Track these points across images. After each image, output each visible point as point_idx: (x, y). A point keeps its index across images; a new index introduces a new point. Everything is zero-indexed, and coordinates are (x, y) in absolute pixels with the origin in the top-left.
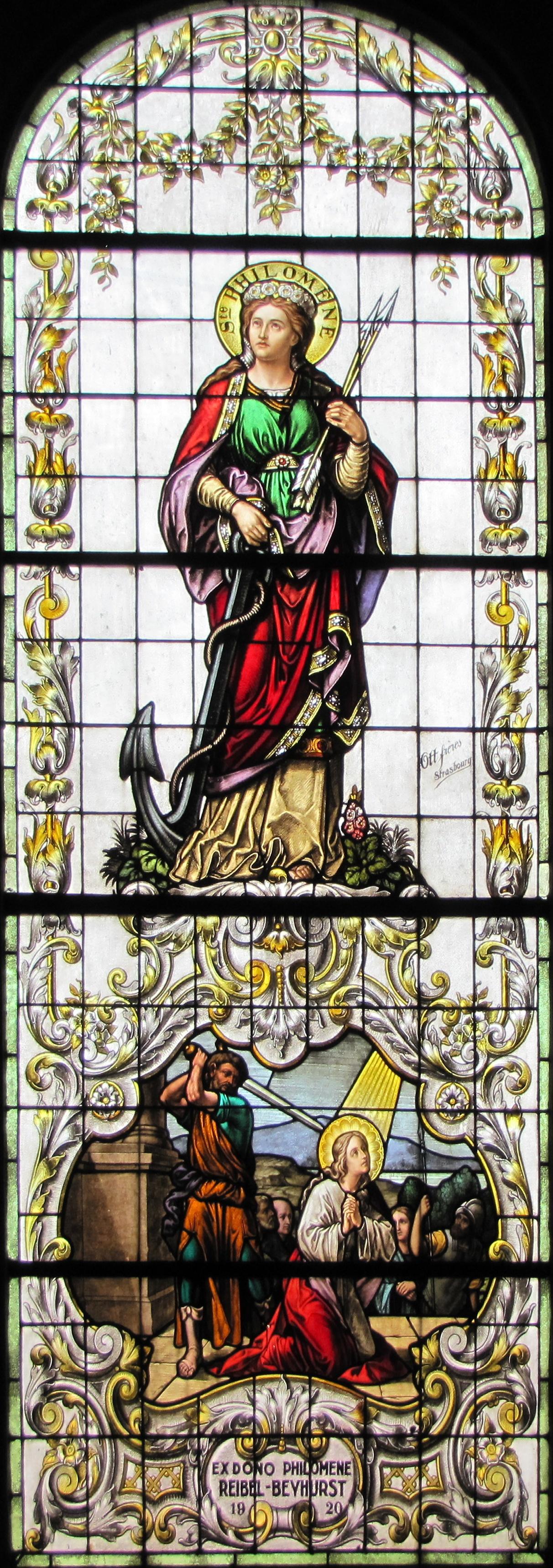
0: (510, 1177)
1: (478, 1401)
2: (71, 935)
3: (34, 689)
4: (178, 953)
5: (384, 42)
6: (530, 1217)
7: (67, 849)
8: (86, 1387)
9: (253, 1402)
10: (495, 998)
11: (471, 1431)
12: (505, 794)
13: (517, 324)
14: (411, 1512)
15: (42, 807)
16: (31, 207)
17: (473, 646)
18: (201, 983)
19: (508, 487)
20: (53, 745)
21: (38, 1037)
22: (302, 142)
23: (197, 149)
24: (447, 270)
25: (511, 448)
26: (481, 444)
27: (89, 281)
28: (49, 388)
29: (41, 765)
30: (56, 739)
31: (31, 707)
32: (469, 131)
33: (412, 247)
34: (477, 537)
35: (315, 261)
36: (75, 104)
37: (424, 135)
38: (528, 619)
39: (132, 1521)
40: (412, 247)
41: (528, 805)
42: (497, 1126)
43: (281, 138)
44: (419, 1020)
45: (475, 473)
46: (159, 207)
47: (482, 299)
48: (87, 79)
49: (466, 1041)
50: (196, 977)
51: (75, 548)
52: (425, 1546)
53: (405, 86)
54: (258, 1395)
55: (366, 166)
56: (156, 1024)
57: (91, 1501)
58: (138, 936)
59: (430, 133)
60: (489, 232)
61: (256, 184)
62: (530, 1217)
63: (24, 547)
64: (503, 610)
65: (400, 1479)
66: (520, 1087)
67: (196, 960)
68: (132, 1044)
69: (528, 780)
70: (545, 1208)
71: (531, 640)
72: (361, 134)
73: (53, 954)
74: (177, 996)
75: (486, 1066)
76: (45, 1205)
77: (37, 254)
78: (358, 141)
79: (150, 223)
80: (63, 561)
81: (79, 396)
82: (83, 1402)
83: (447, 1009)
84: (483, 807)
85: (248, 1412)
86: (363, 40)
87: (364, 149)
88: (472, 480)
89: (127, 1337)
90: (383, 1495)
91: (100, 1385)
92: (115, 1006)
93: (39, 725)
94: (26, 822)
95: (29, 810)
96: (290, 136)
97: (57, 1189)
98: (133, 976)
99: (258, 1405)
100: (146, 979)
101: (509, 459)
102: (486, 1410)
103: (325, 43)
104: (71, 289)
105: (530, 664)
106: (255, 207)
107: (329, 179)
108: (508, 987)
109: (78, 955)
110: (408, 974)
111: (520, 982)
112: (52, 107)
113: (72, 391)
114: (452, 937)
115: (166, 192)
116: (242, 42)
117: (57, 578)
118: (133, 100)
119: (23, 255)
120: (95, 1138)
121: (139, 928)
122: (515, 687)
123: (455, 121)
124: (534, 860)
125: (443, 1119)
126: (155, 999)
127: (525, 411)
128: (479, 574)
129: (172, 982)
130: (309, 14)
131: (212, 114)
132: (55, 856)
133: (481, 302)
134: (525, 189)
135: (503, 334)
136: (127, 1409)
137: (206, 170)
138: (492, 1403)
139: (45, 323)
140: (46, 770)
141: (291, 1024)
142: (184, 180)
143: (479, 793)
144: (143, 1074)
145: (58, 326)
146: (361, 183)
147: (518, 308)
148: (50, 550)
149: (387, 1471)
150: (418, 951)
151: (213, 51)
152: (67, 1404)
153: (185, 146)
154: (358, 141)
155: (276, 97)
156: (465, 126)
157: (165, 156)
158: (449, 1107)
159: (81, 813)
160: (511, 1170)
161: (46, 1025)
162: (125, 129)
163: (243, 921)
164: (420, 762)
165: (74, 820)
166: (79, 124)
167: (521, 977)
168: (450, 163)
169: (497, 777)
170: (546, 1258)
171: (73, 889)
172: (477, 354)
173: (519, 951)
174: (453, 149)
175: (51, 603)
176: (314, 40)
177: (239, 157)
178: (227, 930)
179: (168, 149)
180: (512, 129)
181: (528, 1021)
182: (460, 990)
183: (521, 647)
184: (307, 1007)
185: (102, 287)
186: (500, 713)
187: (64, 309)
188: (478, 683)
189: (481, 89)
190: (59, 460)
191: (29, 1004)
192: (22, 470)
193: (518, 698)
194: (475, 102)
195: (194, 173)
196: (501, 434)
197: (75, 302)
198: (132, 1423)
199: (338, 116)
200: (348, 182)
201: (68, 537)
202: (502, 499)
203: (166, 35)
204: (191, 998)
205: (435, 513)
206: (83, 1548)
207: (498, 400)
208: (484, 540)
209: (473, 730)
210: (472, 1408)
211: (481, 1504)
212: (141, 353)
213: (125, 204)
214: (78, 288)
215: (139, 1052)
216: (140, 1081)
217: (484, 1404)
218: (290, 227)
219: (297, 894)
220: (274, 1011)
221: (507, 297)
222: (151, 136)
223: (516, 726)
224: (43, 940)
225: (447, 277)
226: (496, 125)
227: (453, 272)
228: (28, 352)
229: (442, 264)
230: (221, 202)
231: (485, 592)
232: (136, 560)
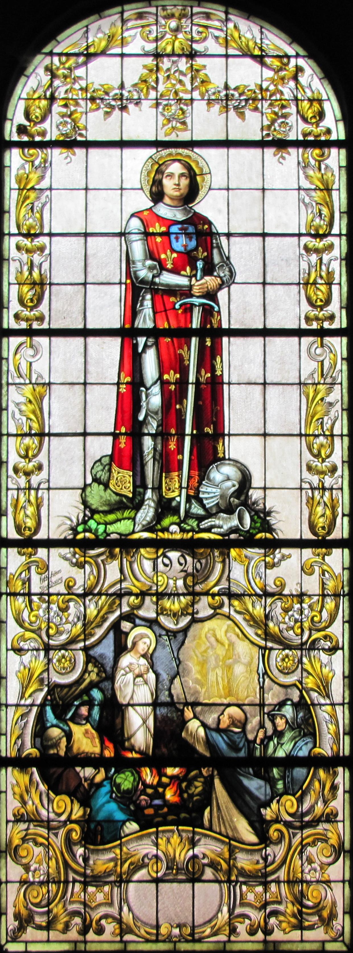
7: (38, 507)
8: (48, 834)
9: (157, 845)
16: (17, 317)
18: (124, 585)
19: (323, 288)
21: (20, 622)
22: (192, 89)
34: (303, 317)
36: (49, 69)
39: (78, 920)
41: (336, 475)
48: (57, 50)
50: (121, 581)
52: (269, 938)
53: (257, 52)
54: (160, 840)
57: (51, 907)
61: (163, 115)
63: (14, 325)
65: (253, 894)
67: (122, 571)
68: (80, 625)
72: (229, 83)
73: (29, 569)
75: (310, 636)
78: (227, 87)
81: (51, 235)
82: (46, 843)
90: (242, 905)
91: (57, 833)
98: (80, 582)
99: (160, 847)
100: (89, 582)
101: (324, 268)
102: (309, 848)
106: (162, 129)
107: (208, 111)
112: (34, 70)
115: (105, 120)
122: (328, 399)
129: (105, 586)
130: (196, 10)
131: (134, 70)
132: (30, 510)
134: (332, 109)
136: (75, 848)
137: (131, 107)
138: (313, 844)
140: (26, 456)
143: (304, 468)
144: (87, 643)
146: (229, 113)
152: (36, 843)
153: (117, 91)
154: (227, 87)
155: (175, 59)
156: (295, 78)
162: (80, 82)
166: (51, 79)
167: (332, 582)
169: (315, 456)
170: (347, 752)
172: (304, 202)
174: (286, 91)
182: (291, 588)
188: (303, 397)
192: (13, 280)
194: (301, 62)
195: (123, 108)
198: (78, 857)
199: (214, 70)
200: (221, 113)
201: (41, 319)
206: (45, 938)
208: (308, 319)
211: (304, 910)
212: (88, 209)
217: (308, 844)
218: (185, 136)
222: (96, 86)
230: (142, 122)
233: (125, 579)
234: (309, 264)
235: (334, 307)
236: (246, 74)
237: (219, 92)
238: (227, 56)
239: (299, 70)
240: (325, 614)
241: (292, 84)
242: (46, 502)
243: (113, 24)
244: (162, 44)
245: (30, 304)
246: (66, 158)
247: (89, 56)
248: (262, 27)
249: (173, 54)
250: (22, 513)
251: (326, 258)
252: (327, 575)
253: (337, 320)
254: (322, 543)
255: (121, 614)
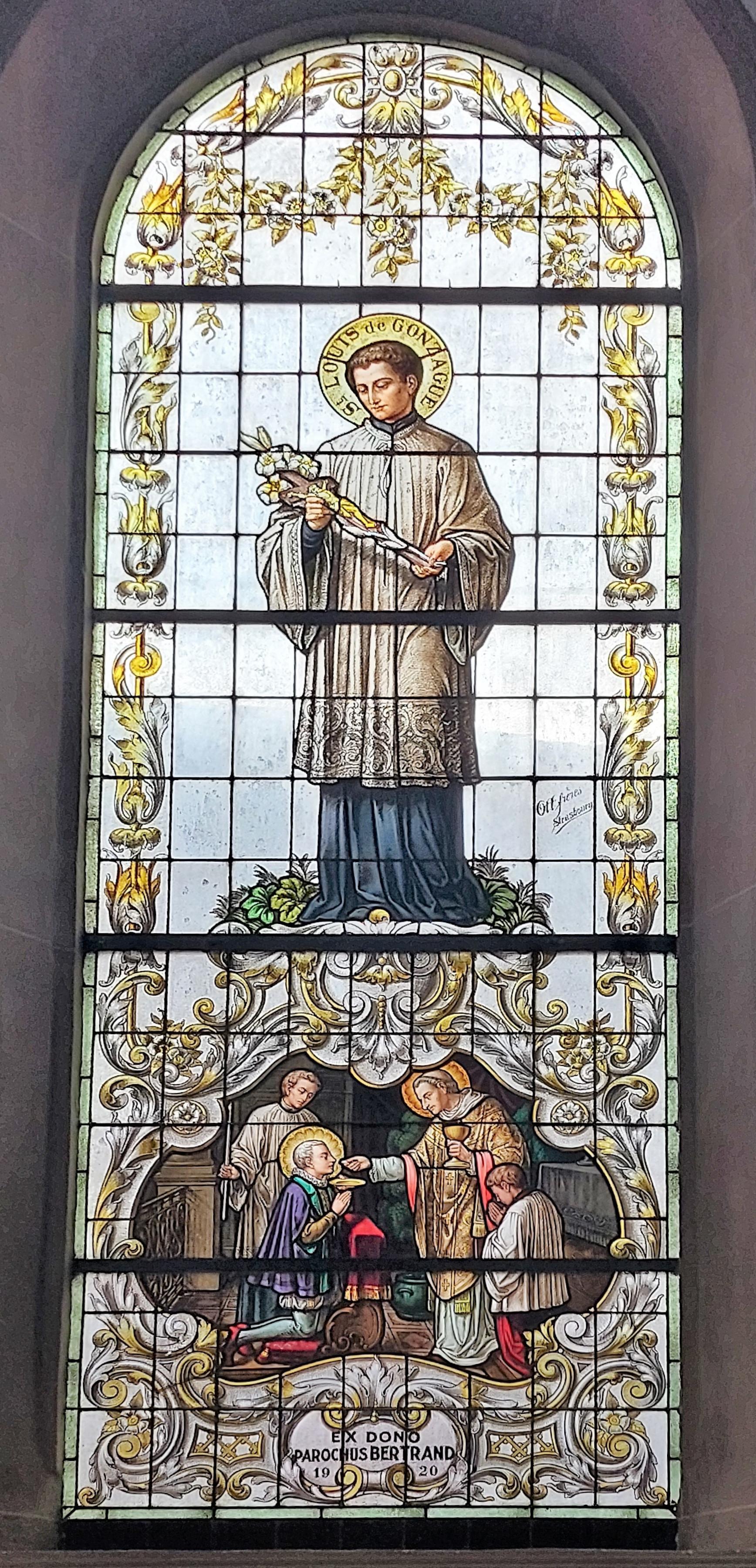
0: (633, 1183)
1: (598, 1379)
2: (154, 970)
3: (120, 743)
4: (272, 985)
5: (513, 83)
6: (658, 1218)
10: (618, 1023)
11: (592, 1404)
12: (627, 838)
13: (649, 377)
14: (524, 1474)
15: (127, 854)
17: (596, 698)
20: (140, 794)
23: (310, 200)
24: (575, 321)
25: (641, 502)
26: (609, 500)
27: (192, 335)
28: (145, 444)
29: (127, 815)
30: (143, 790)
31: (118, 760)
32: (600, 177)
33: (537, 297)
35: (434, 314)
37: (552, 180)
38: (656, 669)
40: (537, 297)
42: (621, 1139)
43: (398, 187)
44: (534, 1043)
45: (601, 529)
46: (268, 260)
47: (610, 349)
49: (584, 1062)
51: (168, 605)
53: (532, 129)
55: (489, 214)
56: (245, 1049)
58: (227, 970)
59: (558, 178)
60: (621, 282)
62: (658, 1218)
63: (114, 603)
64: (629, 661)
66: (647, 1104)
69: (655, 824)
70: (675, 1207)
71: (658, 691)
72: (484, 181)
73: (134, 986)
74: (266, 1026)
76: (117, 1209)
77: (136, 306)
78: (481, 188)
79: (255, 275)
80: (156, 618)
83: (565, 1034)
84: (604, 850)
85: (337, 1387)
86: (488, 76)
87: (487, 196)
88: (597, 536)
89: (203, 1322)
92: (202, 1032)
93: (126, 778)
94: (109, 870)
95: (112, 857)
96: (408, 183)
97: (129, 1199)
103: (447, 82)
104: (172, 342)
105: (657, 716)
108: (632, 1014)
109: (162, 986)
110: (520, 1002)
111: (645, 1010)
113: (169, 449)
114: (570, 982)
116: (359, 82)
117: (149, 636)
118: (242, 146)
119: (121, 308)
120: (174, 1151)
121: (229, 966)
123: (586, 165)
124: (661, 900)
125: (559, 1132)
126: (245, 1028)
127: (656, 465)
128: (603, 628)
132: (138, 900)
133: (610, 353)
135: (634, 386)
139: (143, 378)
141: (393, 1049)
142: (294, 233)
143: (600, 837)
145: (157, 380)
147: (649, 358)
148: (142, 608)
149: (494, 1439)
150: (534, 981)
151: (329, 92)
153: (296, 195)
154: (481, 188)
156: (597, 172)
157: (276, 207)
158: (566, 1121)
159: (170, 860)
160: (635, 1177)
161: (124, 1053)
163: (342, 957)
164: (535, 809)
165: (161, 868)
168: (581, 210)
171: (159, 929)
173: (644, 981)
175: (142, 661)
176: (437, 79)
177: (354, 206)
178: (325, 964)
179: (279, 200)
180: (646, 174)
181: (654, 1044)
182: (579, 1016)
183: (647, 697)
184: (411, 1033)
185: (205, 339)
186: (624, 762)
187: (164, 364)
188: (601, 735)
189: (613, 129)
190: (154, 516)
191: (105, 1033)
193: (644, 746)
194: (608, 146)
196: (627, 488)
197: (176, 356)
199: (462, 162)
200: (470, 231)
202: (631, 554)
203: (277, 76)
204: (284, 1026)
205: (559, 572)
207: (628, 456)
209: (595, 778)
210: (593, 1384)
213: (232, 259)
214: (180, 341)
215: (225, 1074)
216: (225, 1100)
218: (407, 278)
219: (403, 932)
220: (374, 1037)
221: (640, 347)
223: (641, 775)
224: (123, 976)
225: (575, 327)
226: (630, 170)
227: (582, 323)
228: (124, 407)
229: (570, 313)
230: (334, 255)
231: (608, 645)
232: (234, 617)
233: (297, 1004)
234: (614, 509)
235: (655, 824)
236: (514, 167)
237: (468, 196)
238: (481, 137)
239: (603, 159)
240: (634, 1051)
241: (592, 182)
242: (164, 887)
243: (289, 75)
244: (372, 111)
245: (142, 571)
246: (205, 333)
247: (247, 137)
248: (542, 84)
249: (392, 440)
250: (125, 901)
251: (642, 500)
252: (637, 995)
253: (660, 272)
254: (631, 945)
255: (288, 1053)
